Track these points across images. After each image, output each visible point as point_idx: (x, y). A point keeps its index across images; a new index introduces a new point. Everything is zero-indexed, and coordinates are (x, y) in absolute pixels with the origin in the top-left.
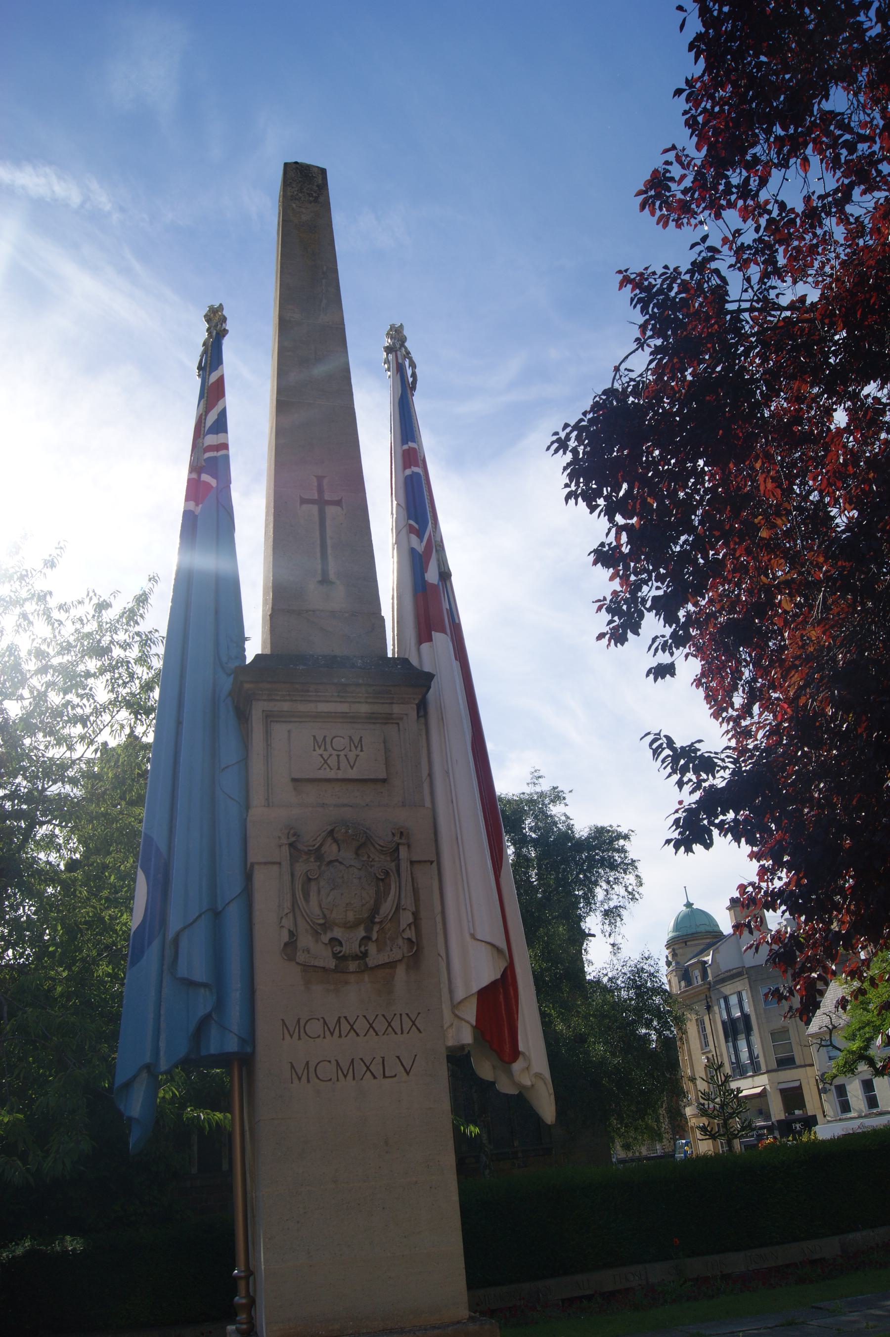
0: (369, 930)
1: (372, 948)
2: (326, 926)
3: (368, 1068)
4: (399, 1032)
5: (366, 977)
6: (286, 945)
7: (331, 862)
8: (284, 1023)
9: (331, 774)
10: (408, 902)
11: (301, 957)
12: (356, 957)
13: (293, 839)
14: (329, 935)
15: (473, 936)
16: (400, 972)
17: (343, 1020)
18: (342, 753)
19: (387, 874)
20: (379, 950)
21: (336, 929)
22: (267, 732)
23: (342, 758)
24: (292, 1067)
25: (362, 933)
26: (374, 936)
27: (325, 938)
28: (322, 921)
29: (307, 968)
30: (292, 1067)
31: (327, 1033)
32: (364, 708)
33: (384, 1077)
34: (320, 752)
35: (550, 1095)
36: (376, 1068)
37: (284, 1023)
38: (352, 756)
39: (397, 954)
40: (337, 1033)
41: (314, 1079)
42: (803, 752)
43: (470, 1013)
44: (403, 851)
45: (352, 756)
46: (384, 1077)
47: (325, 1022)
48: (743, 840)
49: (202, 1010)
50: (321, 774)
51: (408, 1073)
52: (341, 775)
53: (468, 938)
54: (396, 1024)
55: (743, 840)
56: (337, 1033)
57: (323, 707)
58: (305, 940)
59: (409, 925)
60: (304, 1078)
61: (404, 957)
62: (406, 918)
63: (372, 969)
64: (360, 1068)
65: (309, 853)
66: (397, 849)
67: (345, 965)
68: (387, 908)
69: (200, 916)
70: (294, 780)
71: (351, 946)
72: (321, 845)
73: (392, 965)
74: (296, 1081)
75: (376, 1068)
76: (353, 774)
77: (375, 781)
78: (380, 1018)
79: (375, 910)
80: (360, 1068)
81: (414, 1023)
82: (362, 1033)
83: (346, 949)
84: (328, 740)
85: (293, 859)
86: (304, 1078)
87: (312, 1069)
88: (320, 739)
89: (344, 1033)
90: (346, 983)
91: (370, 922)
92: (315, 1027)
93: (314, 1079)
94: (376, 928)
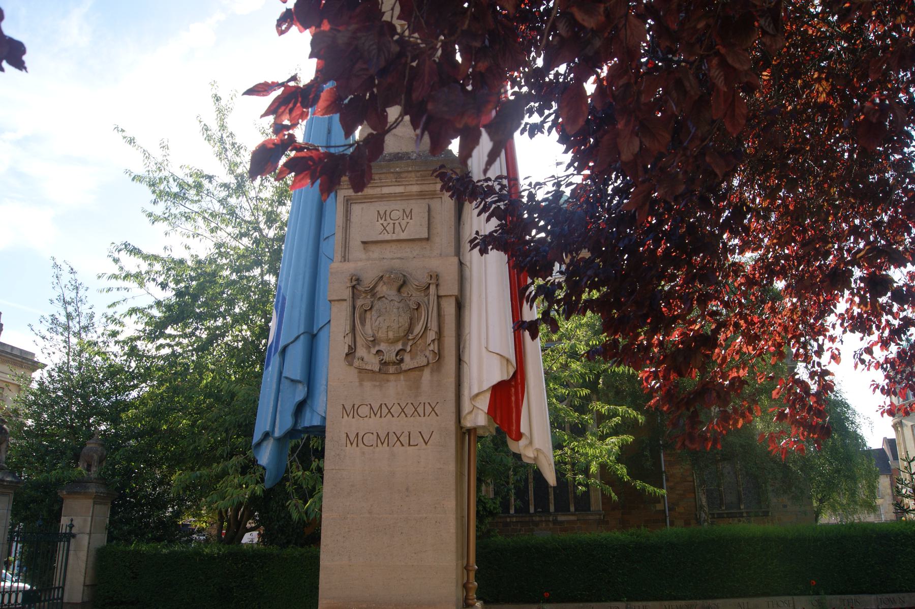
0: (405, 344)
1: (407, 358)
2: (375, 342)
3: (398, 439)
4: (422, 415)
5: (402, 377)
6: (347, 355)
7: (380, 298)
8: (344, 407)
9: (387, 237)
10: (433, 325)
11: (357, 363)
12: (394, 363)
13: (354, 283)
14: (377, 348)
15: (486, 348)
16: (427, 373)
17: (383, 406)
18: (397, 222)
19: (419, 306)
20: (412, 359)
21: (382, 344)
22: (347, 211)
23: (397, 225)
24: (347, 436)
25: (400, 347)
26: (408, 349)
27: (374, 351)
28: (372, 339)
29: (361, 370)
30: (347, 436)
31: (372, 415)
32: (415, 189)
33: (409, 445)
34: (381, 222)
35: (550, 464)
36: (404, 439)
37: (344, 407)
38: (404, 223)
39: (422, 361)
40: (379, 414)
41: (361, 444)
42: (372, 94)
43: (484, 403)
44: (432, 289)
45: (404, 223)
46: (409, 445)
47: (371, 408)
48: (319, 181)
49: (299, 397)
50: (381, 238)
51: (426, 444)
52: (394, 237)
53: (484, 350)
54: (420, 410)
55: (319, 181)
56: (379, 414)
57: (386, 190)
58: (361, 352)
59: (433, 341)
60: (355, 444)
61: (428, 364)
62: (432, 335)
63: (405, 371)
64: (393, 439)
65: (366, 292)
66: (428, 287)
67: (389, 367)
68: (418, 329)
69: (297, 338)
70: (364, 243)
71: (390, 356)
72: (374, 287)
73: (420, 369)
74: (349, 445)
75: (404, 439)
76: (403, 236)
77: (420, 240)
78: (410, 405)
79: (410, 329)
80: (393, 439)
81: (433, 409)
82: (396, 415)
83: (386, 358)
84: (388, 213)
85: (354, 297)
86: (355, 444)
87: (360, 438)
88: (382, 213)
89: (383, 415)
90: (388, 381)
91: (405, 338)
92: (364, 410)
93: (361, 444)
94: (410, 343)
